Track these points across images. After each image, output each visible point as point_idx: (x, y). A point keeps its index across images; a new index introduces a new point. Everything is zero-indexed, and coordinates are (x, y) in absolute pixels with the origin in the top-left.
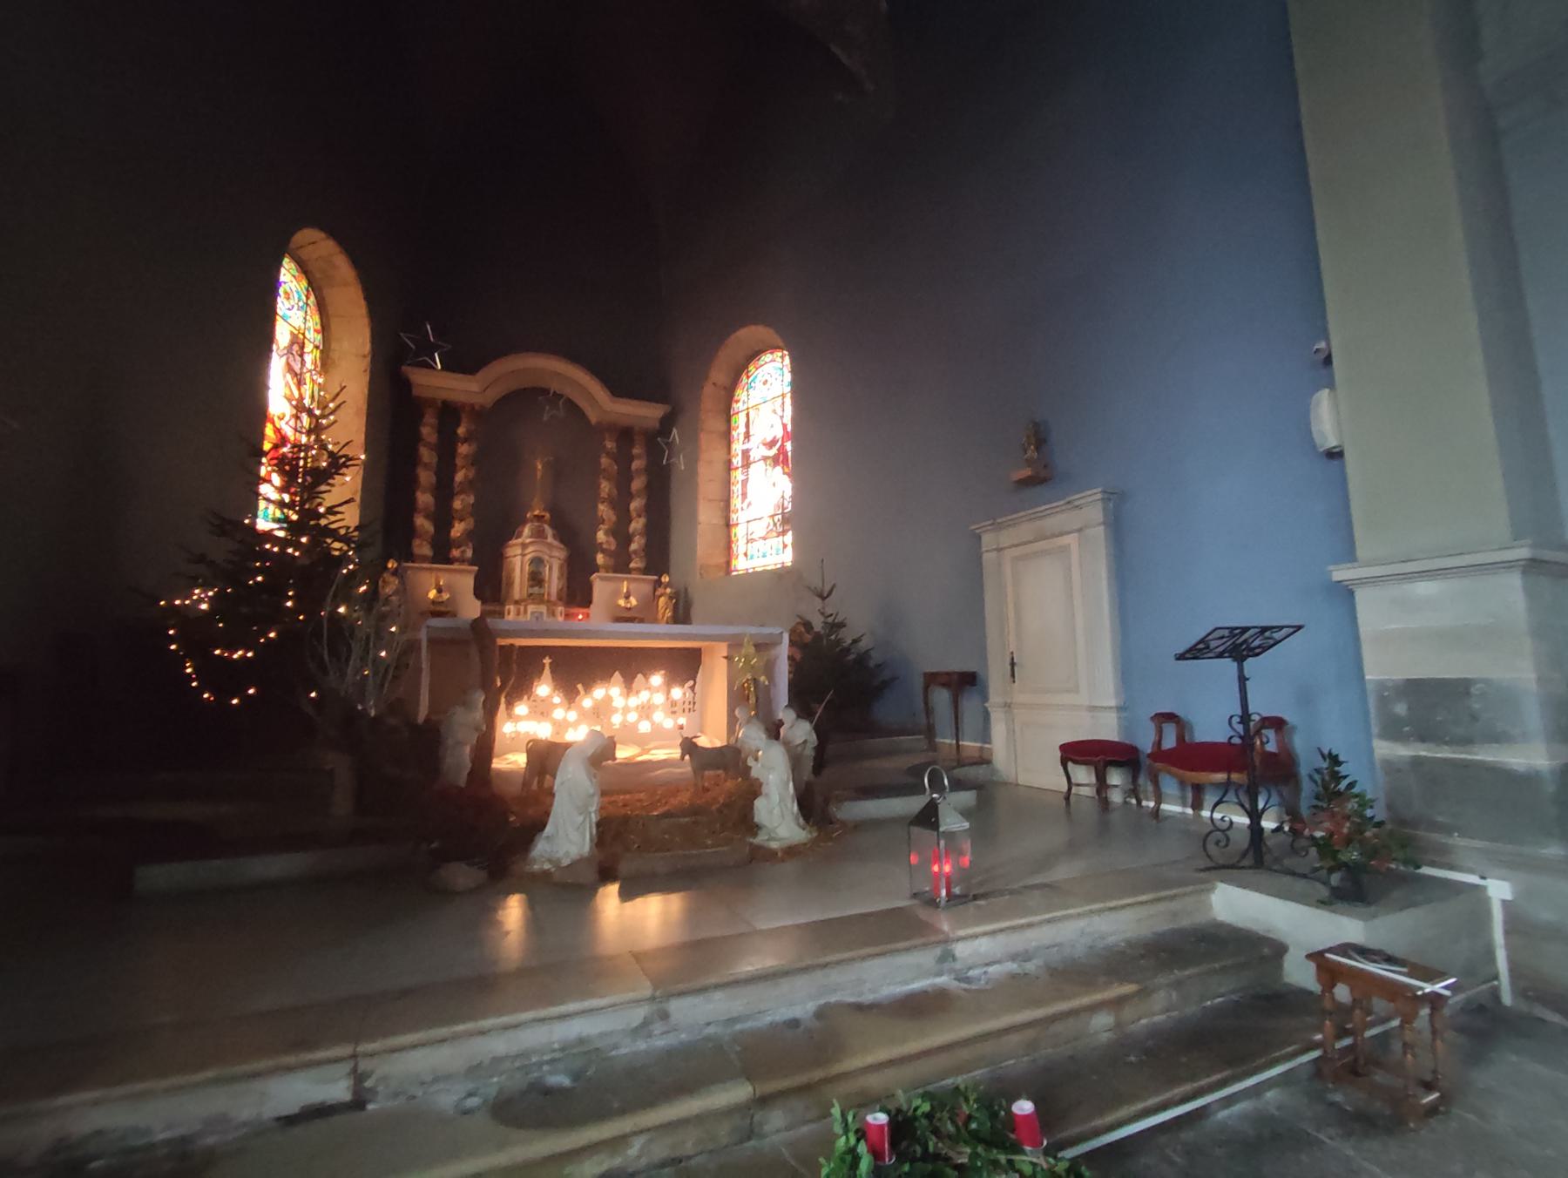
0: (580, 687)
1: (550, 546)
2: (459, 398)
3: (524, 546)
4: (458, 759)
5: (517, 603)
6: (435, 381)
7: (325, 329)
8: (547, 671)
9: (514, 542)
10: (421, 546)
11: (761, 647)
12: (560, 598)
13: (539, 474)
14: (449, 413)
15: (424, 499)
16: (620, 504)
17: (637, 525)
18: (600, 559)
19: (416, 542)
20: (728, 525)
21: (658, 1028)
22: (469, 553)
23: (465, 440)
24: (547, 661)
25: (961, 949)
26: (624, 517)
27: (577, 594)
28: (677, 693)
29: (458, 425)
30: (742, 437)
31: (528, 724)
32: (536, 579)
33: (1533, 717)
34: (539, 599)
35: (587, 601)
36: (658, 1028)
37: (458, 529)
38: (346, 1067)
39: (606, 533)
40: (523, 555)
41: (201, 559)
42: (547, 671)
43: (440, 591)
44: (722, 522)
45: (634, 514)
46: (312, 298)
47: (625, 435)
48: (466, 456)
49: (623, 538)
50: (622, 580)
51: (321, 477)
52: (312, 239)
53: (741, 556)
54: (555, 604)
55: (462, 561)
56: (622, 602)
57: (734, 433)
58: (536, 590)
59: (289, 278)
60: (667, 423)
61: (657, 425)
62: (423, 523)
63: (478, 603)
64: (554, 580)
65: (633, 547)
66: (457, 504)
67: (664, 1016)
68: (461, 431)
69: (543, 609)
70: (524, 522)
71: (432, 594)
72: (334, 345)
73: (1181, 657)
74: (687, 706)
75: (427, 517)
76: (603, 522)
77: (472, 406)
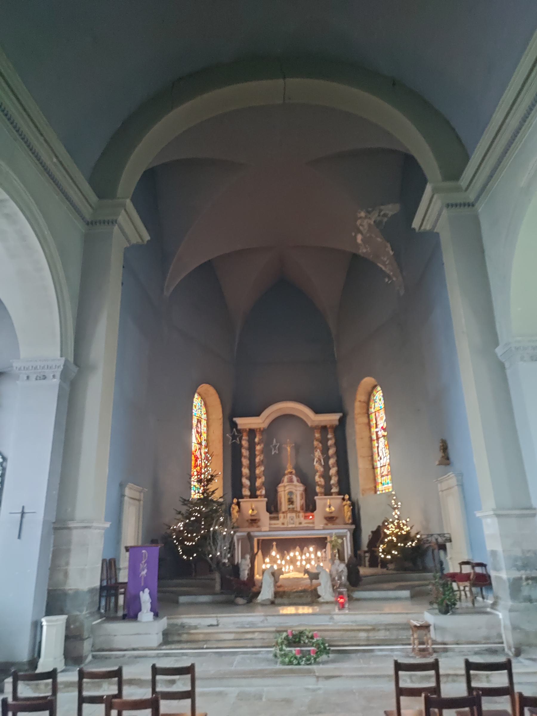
0: (285, 552)
1: (296, 486)
2: (253, 427)
3: (285, 486)
4: (245, 574)
5: (283, 513)
6: (243, 423)
7: (207, 413)
8: (275, 547)
9: (280, 485)
10: (245, 491)
11: (341, 537)
12: (302, 508)
13: (289, 454)
14: (252, 432)
15: (245, 471)
16: (325, 450)
17: (333, 471)
18: (318, 489)
19: (244, 490)
20: (374, 468)
21: (265, 622)
22: (264, 492)
23: (259, 443)
24: (274, 543)
25: (335, 617)
26: (327, 468)
27: (310, 507)
28: (319, 554)
29: (255, 437)
30: (375, 425)
31: (264, 565)
32: (291, 501)
33: (502, 563)
34: (293, 510)
35: (314, 509)
36: (265, 622)
37: (258, 483)
38: (215, 619)
39: (320, 477)
40: (284, 491)
41: (180, 513)
42: (275, 547)
43: (253, 510)
44: (371, 467)
45: (331, 466)
46: (203, 402)
47: (324, 429)
48: (259, 450)
49: (326, 476)
50: (327, 499)
51: (209, 481)
52: (205, 388)
53: (380, 485)
54: (299, 512)
55: (261, 496)
56: (328, 509)
57: (372, 423)
58: (291, 506)
59: (197, 401)
60: (342, 421)
61: (337, 423)
62: (246, 482)
63: (268, 514)
64: (299, 501)
65: (332, 482)
66: (257, 472)
67: (267, 620)
68: (257, 440)
69: (294, 515)
70: (284, 475)
71: (250, 511)
72: (210, 417)
73: (19, 537)
74: (323, 559)
75: (247, 478)
76: (317, 471)
77: (260, 429)
